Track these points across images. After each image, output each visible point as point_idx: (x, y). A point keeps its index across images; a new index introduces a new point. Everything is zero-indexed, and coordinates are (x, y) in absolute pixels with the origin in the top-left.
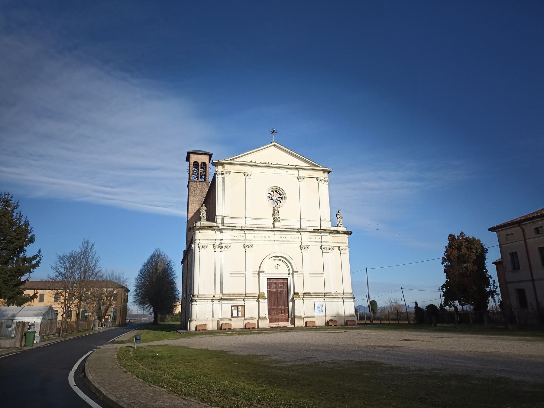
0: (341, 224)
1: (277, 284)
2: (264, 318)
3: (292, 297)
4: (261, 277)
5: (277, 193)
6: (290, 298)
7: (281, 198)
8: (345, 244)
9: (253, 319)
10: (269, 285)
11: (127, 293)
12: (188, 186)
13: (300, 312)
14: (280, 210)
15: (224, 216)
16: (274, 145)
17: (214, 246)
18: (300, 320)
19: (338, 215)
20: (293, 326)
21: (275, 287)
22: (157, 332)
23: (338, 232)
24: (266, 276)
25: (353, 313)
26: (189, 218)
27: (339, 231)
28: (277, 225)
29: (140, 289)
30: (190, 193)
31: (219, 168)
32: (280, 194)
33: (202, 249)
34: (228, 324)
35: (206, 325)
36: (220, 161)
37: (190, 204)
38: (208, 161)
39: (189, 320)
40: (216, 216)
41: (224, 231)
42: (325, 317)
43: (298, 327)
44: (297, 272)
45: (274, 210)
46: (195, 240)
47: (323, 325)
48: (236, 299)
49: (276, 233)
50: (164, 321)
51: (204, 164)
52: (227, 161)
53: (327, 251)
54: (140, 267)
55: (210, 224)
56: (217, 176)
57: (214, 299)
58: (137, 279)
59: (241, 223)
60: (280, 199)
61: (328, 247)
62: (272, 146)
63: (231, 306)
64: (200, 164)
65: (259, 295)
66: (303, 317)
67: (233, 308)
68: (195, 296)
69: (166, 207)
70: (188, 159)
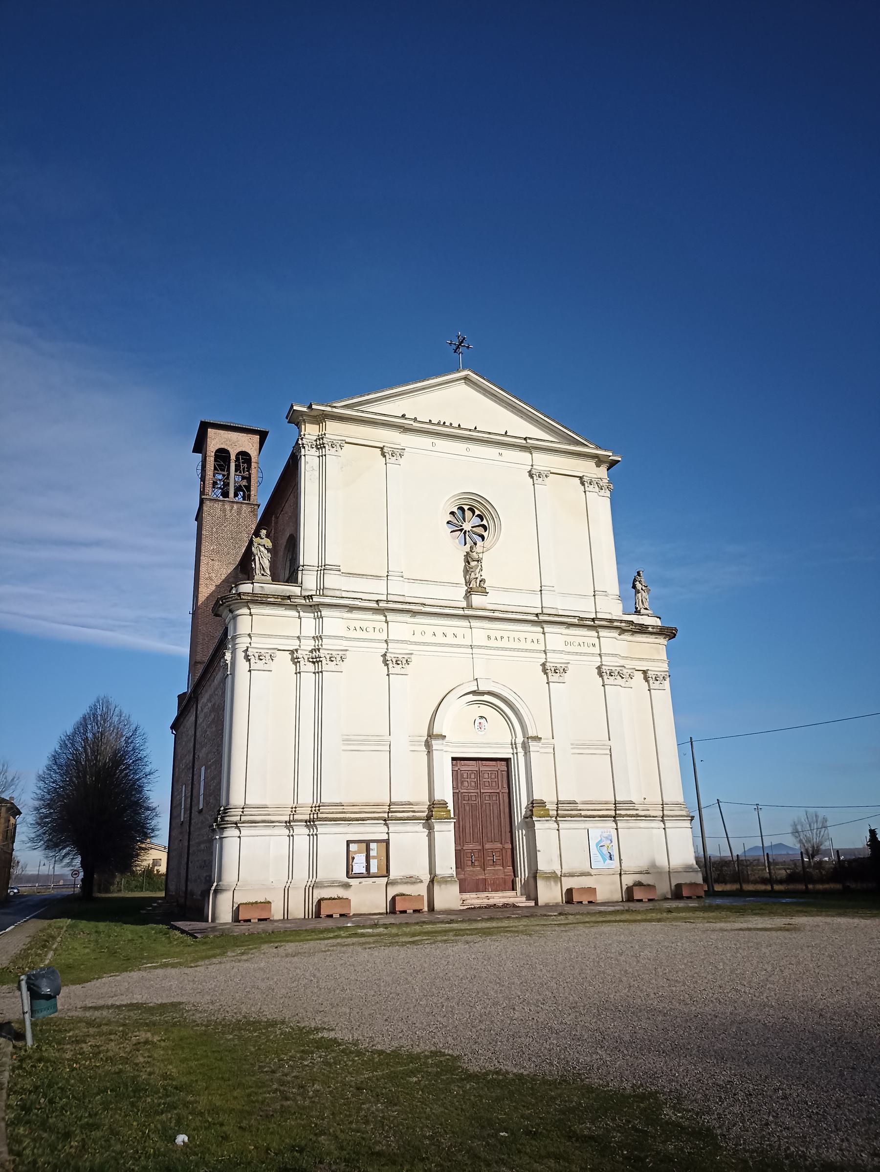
0: (646, 609)
1: (478, 773)
2: (445, 881)
3: (523, 813)
4: (435, 754)
5: (474, 512)
6: (518, 819)
7: (484, 527)
8: (660, 664)
9: (414, 883)
10: (455, 775)
11: (15, 818)
12: (199, 517)
13: (552, 860)
14: (485, 558)
15: (323, 568)
16: (466, 379)
17: (295, 656)
18: (552, 883)
19: (638, 582)
20: (532, 904)
21: (473, 784)
22: (102, 926)
23: (642, 629)
24: (450, 749)
25: (691, 863)
26: (202, 598)
27: (647, 627)
28: (476, 600)
29: (49, 806)
30: (204, 532)
31: (310, 431)
32: (481, 517)
33: (256, 664)
34: (339, 898)
35: (269, 903)
36: (314, 407)
37: (204, 560)
38: (256, 449)
39: (213, 888)
40: (301, 568)
41: (325, 612)
42: (620, 874)
43: (547, 906)
44: (537, 739)
45: (468, 558)
46: (234, 638)
47: (615, 900)
48: (363, 819)
49: (475, 623)
50: (108, 891)
51: (244, 457)
52: (335, 410)
53: (616, 682)
54: (52, 745)
55: (283, 590)
56: (303, 452)
57: (294, 821)
58: (41, 779)
59: (376, 589)
60: (480, 530)
61: (618, 669)
62: (457, 380)
63: (348, 843)
64: (233, 457)
65: (430, 809)
66: (559, 874)
67: (353, 847)
68: (233, 812)
69: (111, 630)
70: (200, 446)
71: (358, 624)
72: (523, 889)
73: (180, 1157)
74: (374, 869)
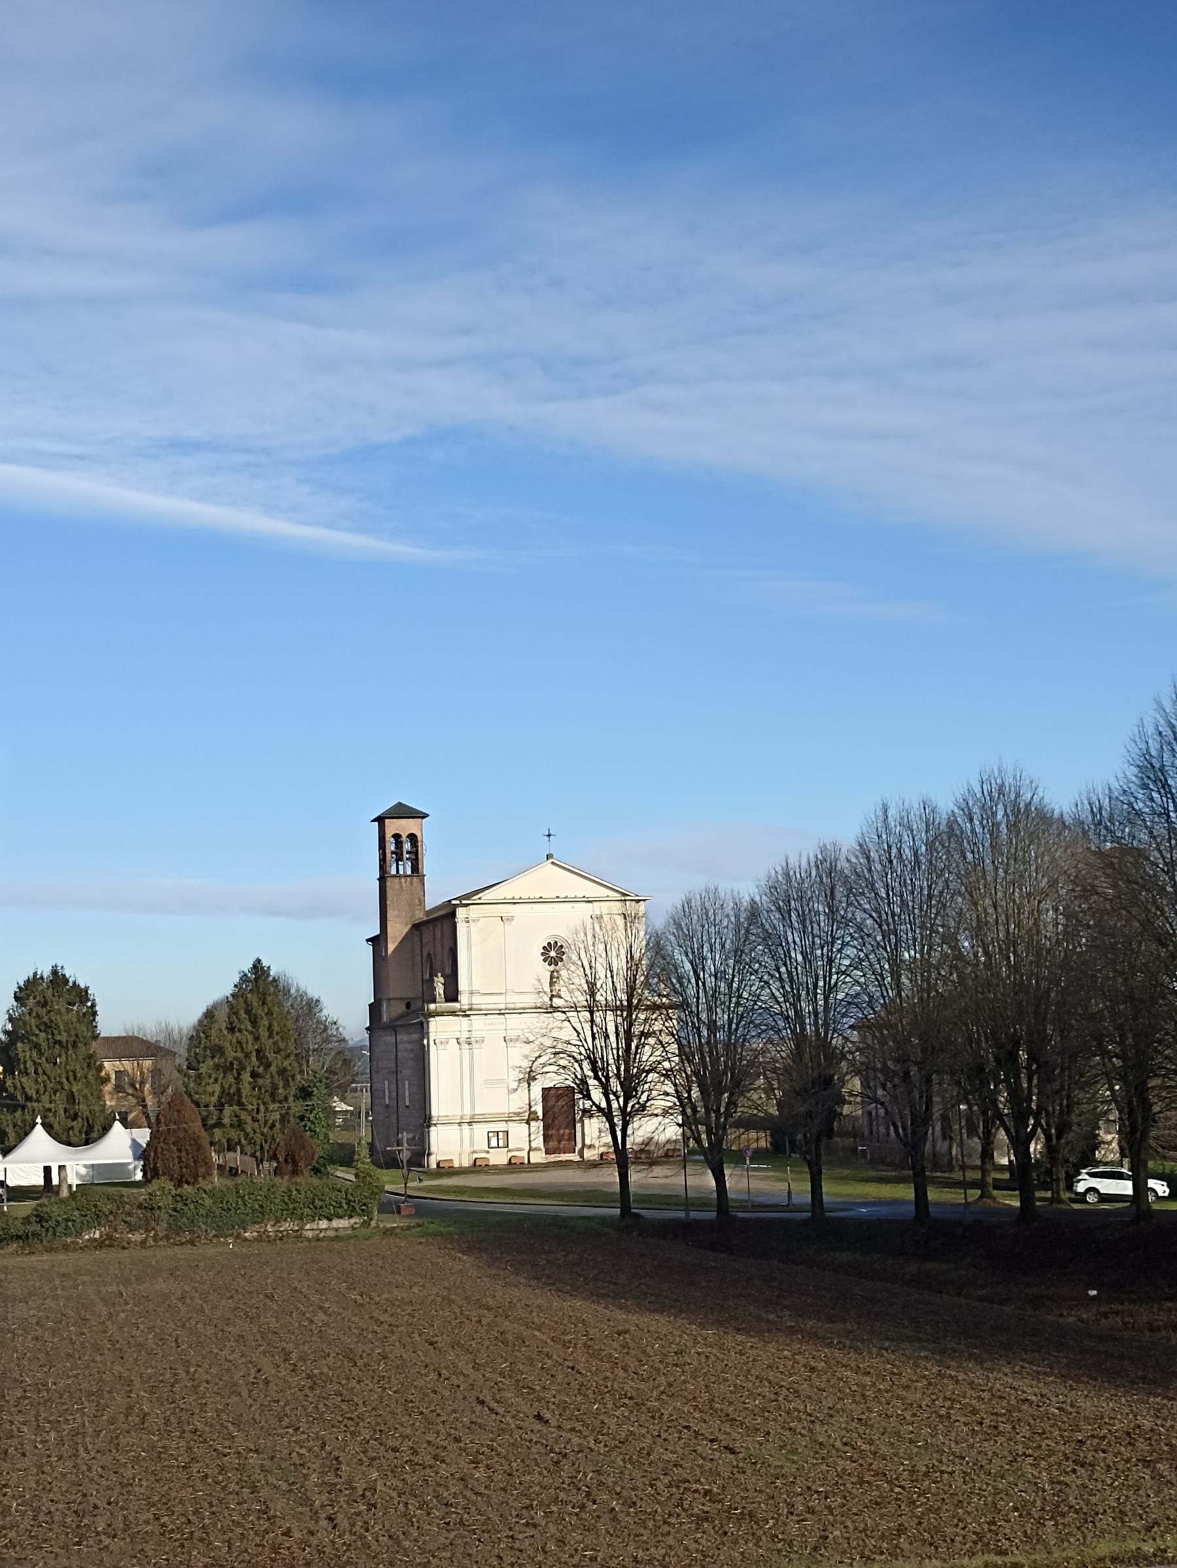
2: (536, 1149)
59: (499, 1002)
67: (490, 1134)
71: (490, 1022)
72: (498, 1219)
73: (1022, 1001)
74: (501, 1144)
